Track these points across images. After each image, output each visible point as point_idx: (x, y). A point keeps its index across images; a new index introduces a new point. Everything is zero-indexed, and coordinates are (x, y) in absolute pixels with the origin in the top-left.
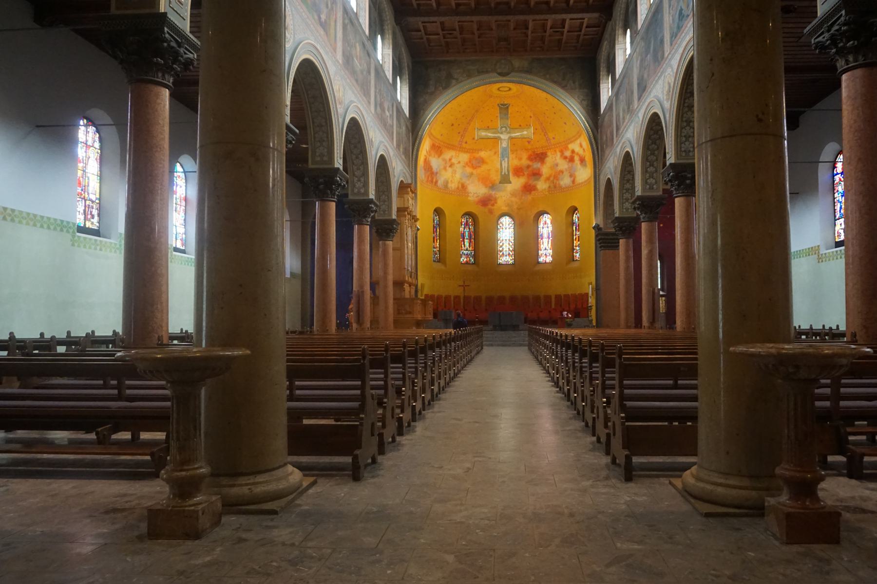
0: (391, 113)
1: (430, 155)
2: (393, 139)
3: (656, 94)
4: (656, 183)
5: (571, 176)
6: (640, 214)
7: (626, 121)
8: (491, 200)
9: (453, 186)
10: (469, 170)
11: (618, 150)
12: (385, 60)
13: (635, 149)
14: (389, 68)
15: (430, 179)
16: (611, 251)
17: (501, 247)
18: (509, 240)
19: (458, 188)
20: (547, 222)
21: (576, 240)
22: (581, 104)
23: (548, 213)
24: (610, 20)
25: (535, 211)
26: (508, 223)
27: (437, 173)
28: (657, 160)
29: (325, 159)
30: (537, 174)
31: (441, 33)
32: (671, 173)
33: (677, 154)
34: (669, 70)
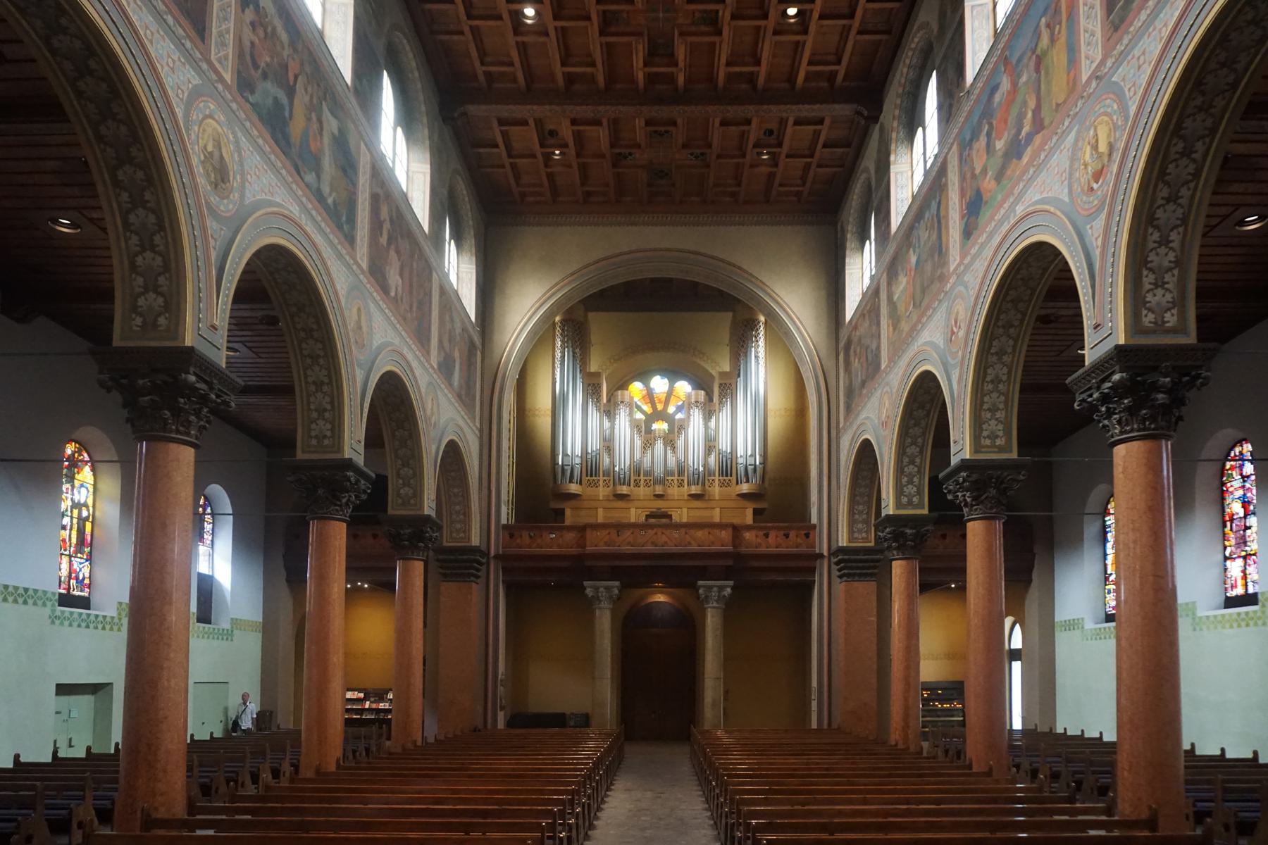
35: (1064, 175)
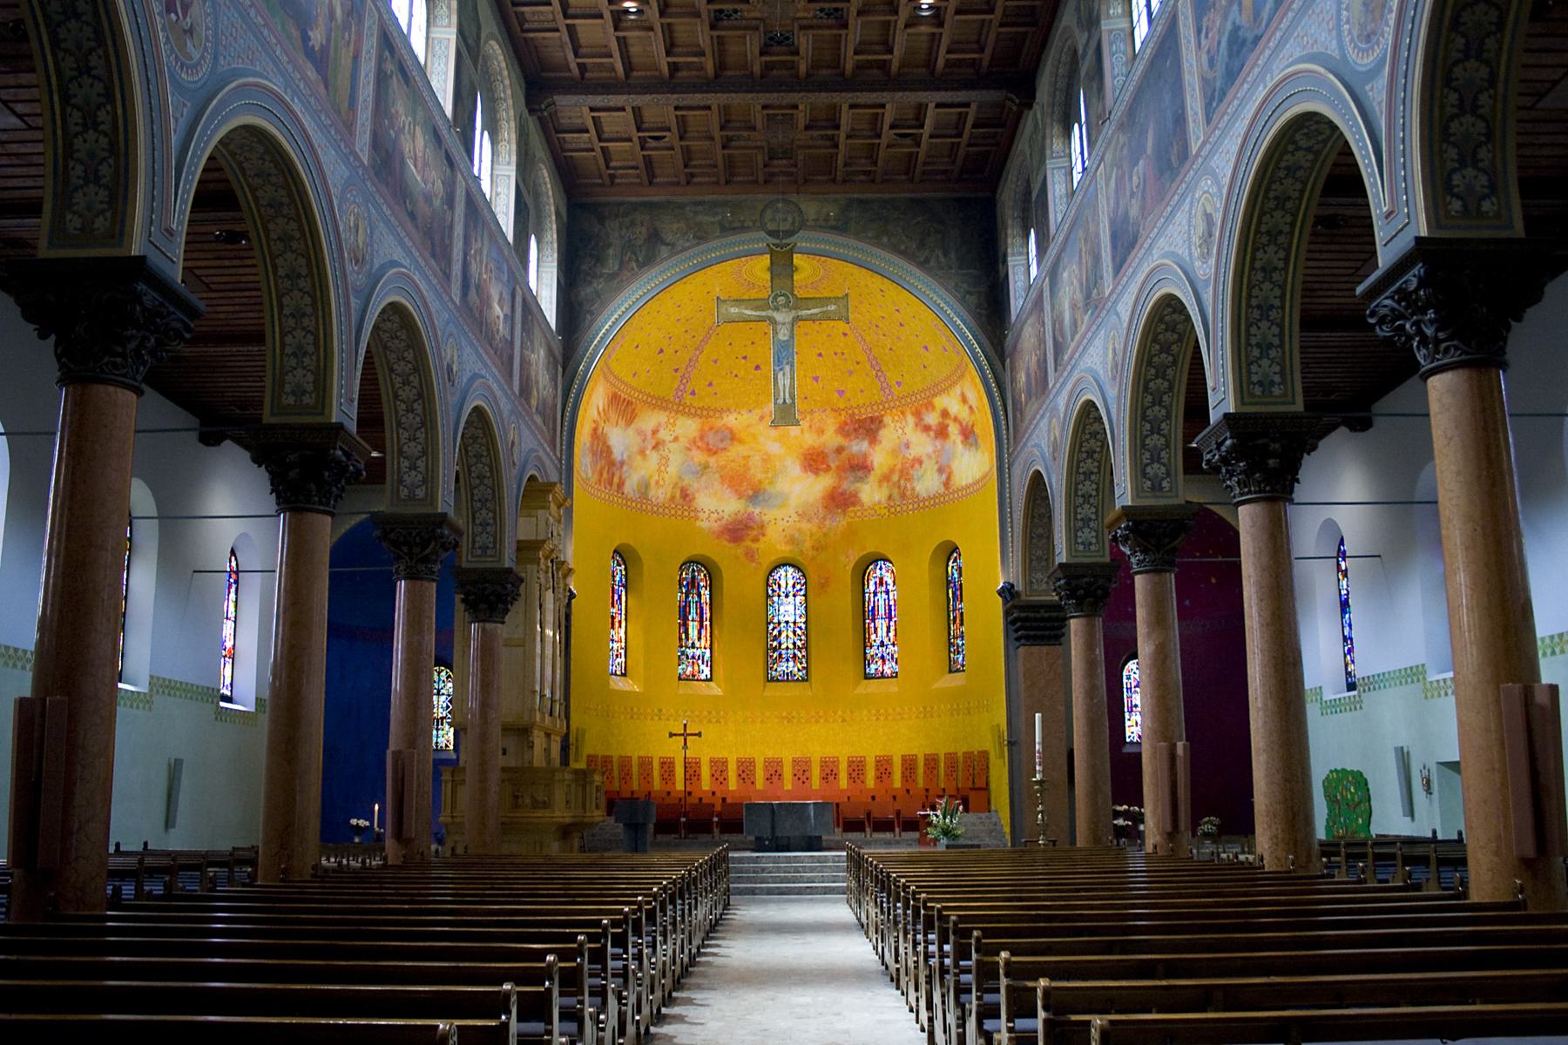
0: (507, 309)
1: (607, 420)
2: (511, 375)
3: (1166, 249)
4: (1168, 474)
5: (940, 470)
6: (1129, 553)
7: (1082, 329)
8: (752, 528)
9: (659, 494)
10: (699, 457)
11: (1062, 401)
12: (499, 190)
13: (1112, 393)
14: (508, 207)
15: (605, 475)
16: (1045, 649)
17: (775, 638)
18: (795, 623)
19: (673, 498)
20: (885, 579)
21: (954, 623)
22: (962, 301)
23: (886, 560)
24: (1030, 106)
25: (855, 556)
26: (791, 582)
27: (622, 463)
28: (1168, 416)
29: (307, 400)
30: (860, 467)
31: (635, 135)
32: (1226, 439)
33: (1242, 392)
34: (1206, 184)
35: (1331, 23)
